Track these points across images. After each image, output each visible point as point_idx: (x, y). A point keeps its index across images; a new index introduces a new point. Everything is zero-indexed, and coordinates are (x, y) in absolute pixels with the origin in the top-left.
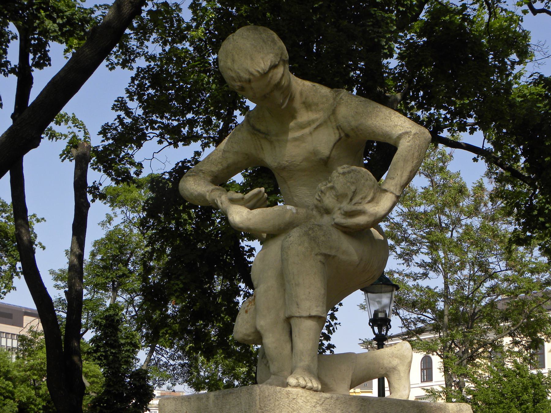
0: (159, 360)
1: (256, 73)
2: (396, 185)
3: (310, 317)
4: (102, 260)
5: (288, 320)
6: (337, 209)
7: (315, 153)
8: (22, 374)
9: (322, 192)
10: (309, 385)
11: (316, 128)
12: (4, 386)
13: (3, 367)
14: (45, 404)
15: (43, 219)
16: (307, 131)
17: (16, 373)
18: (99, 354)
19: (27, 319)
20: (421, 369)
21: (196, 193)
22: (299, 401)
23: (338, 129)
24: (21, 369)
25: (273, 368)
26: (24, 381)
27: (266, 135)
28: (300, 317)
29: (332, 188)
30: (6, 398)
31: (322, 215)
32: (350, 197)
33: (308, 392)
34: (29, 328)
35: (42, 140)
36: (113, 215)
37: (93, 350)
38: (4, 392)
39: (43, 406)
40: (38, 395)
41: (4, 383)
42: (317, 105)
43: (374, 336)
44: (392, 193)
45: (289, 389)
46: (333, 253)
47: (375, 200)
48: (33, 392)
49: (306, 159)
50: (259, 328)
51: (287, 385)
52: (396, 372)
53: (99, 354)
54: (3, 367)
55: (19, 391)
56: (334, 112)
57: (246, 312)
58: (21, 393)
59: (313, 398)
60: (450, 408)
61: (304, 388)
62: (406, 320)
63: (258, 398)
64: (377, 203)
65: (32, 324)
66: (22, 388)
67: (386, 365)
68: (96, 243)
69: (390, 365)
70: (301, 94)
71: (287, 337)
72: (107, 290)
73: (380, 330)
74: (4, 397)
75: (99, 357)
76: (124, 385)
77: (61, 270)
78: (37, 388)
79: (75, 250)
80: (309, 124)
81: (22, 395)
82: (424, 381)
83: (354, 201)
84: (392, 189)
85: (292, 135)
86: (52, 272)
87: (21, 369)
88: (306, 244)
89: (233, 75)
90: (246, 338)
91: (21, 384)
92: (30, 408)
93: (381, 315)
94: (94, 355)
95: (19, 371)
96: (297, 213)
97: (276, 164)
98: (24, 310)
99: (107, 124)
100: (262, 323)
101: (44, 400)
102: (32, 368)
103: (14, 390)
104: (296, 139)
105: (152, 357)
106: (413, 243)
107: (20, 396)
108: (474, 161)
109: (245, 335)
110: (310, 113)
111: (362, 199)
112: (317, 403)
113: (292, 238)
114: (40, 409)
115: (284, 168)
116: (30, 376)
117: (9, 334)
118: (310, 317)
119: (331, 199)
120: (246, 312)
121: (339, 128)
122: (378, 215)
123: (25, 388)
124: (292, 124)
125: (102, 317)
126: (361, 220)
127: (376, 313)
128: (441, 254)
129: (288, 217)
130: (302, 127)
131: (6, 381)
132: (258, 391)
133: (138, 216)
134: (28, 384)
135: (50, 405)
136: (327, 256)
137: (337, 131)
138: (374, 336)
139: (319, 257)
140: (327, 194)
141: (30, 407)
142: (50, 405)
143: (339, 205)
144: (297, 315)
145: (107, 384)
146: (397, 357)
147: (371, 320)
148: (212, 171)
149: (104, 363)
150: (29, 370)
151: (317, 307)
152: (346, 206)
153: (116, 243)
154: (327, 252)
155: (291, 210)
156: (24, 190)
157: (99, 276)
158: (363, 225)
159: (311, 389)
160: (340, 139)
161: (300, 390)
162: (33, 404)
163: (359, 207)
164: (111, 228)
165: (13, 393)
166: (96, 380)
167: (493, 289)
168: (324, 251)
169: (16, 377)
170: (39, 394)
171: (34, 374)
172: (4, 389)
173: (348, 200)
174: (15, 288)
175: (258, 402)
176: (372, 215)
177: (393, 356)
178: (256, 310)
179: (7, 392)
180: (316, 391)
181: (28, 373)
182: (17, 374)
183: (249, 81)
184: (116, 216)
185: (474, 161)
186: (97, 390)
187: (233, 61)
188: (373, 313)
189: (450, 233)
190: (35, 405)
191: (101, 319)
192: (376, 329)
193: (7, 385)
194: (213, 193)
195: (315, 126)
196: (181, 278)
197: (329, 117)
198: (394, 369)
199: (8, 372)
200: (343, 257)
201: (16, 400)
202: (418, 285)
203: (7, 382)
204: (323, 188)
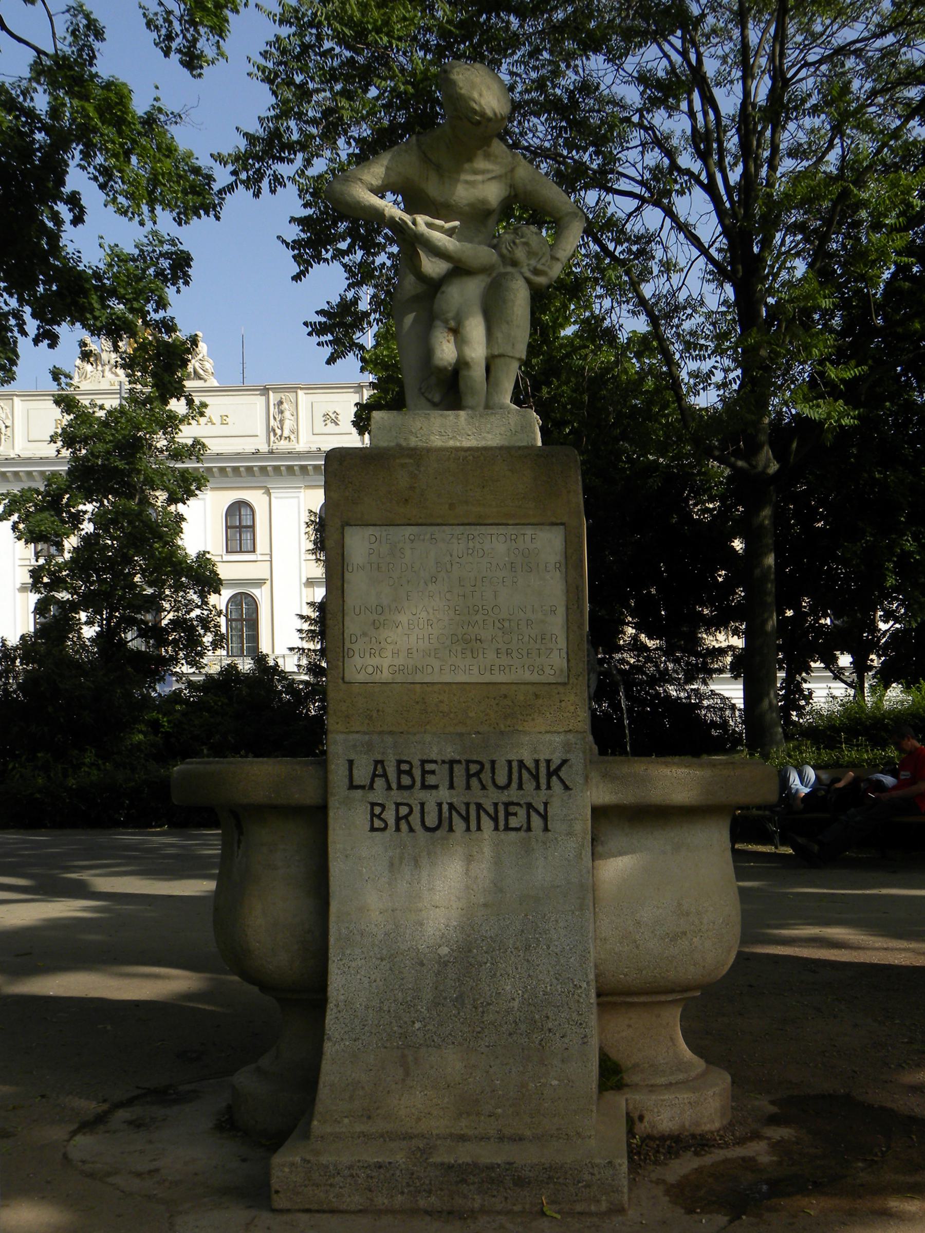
7: (484, 202)
11: (490, 179)
15: (140, 7)
16: (479, 178)
21: (367, 203)
23: (511, 186)
28: (512, 357)
42: (496, 157)
49: (471, 205)
56: (512, 170)
80: (483, 172)
89: (477, 107)
97: (442, 200)
104: (467, 182)
108: (82, 221)
110: (487, 163)
124: (467, 166)
130: (475, 172)
137: (508, 189)
140: (520, 248)
156: (123, 1001)
174: (140, 7)
185: (82, 221)
195: (489, 176)
197: (506, 174)
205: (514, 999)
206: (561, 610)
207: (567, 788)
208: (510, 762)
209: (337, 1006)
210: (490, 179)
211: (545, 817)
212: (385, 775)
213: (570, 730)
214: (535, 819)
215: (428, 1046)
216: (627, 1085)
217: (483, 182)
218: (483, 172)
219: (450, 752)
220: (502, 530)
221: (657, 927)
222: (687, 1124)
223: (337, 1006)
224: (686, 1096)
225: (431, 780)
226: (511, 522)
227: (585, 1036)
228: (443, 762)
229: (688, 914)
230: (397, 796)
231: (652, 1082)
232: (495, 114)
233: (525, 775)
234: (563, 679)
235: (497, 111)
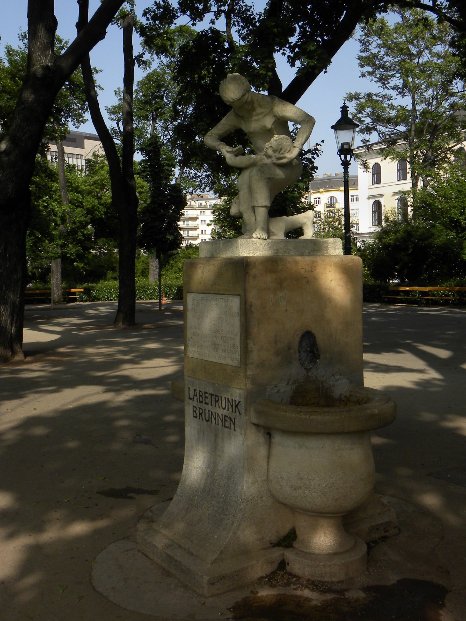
0: (190, 173)
1: (236, 99)
2: (299, 144)
3: (262, 206)
4: (144, 96)
5: (253, 207)
6: (273, 156)
8: (88, 187)
9: (267, 148)
10: (262, 237)
12: (75, 198)
13: (74, 183)
14: (105, 210)
16: (261, 116)
17: (83, 187)
18: (146, 173)
19: (87, 142)
20: (398, 170)
22: (258, 244)
24: (87, 184)
25: (248, 228)
26: (89, 193)
27: (242, 117)
28: (258, 206)
29: (271, 147)
30: (77, 207)
31: (268, 159)
32: (279, 151)
33: (261, 240)
34: (92, 153)
35: (106, 34)
36: (151, 61)
37: (142, 171)
38: (76, 203)
39: (104, 211)
40: (100, 204)
41: (75, 196)
43: (342, 162)
44: (298, 148)
45: (253, 239)
46: (272, 176)
47: (291, 151)
48: (96, 201)
50: (241, 211)
51: (252, 237)
52: (306, 225)
53: (146, 173)
54: (74, 183)
55: (87, 201)
57: (235, 203)
58: (88, 202)
59: (264, 242)
60: (330, 241)
61: (259, 238)
62: (383, 133)
63: (240, 244)
64: (292, 152)
65: (94, 150)
66: (89, 199)
67: (301, 222)
68: (139, 83)
69: (303, 222)
70: (257, 100)
71: (253, 214)
72: (147, 120)
73: (346, 157)
74: (76, 206)
75: (146, 175)
76: (165, 196)
77: (113, 107)
78: (99, 198)
79: (126, 98)
80: (262, 113)
81: (89, 204)
82: (400, 180)
83: (281, 153)
84: (298, 146)
85: (254, 118)
86: (107, 109)
87: (87, 184)
88: (259, 175)
89: (226, 100)
90: (235, 215)
91: (88, 196)
92: (96, 214)
93: (346, 147)
94: (143, 174)
95: (85, 186)
96: (256, 158)
98: (84, 135)
99: (148, 9)
100: (242, 209)
101: (104, 207)
102: (95, 182)
103: (82, 200)
104: (256, 120)
105: (184, 171)
106: (387, 69)
107: (87, 205)
109: (235, 213)
111: (284, 151)
112: (265, 244)
113: (253, 173)
114: (102, 214)
115: (251, 133)
116: (93, 189)
117: (74, 154)
118: (262, 206)
119: (271, 152)
120: (235, 203)
121: (275, 116)
122: (292, 158)
123: (90, 199)
124: (254, 113)
125: (146, 145)
126: (284, 161)
127: (343, 145)
128: (410, 79)
129: (252, 161)
130: (258, 115)
131: (77, 194)
132: (240, 242)
133: (170, 60)
134: (92, 195)
135: (109, 211)
136: (269, 179)
137: (274, 117)
138: (342, 162)
139: (265, 180)
140: (269, 149)
141: (95, 213)
142: (109, 211)
143: (275, 154)
144: (257, 205)
145: (152, 196)
146: (306, 218)
147: (339, 151)
148: (218, 134)
149: (149, 180)
150: (93, 185)
151: (265, 202)
152: (278, 155)
153: (154, 82)
154: (269, 177)
155: (253, 157)
157: (142, 109)
158: (285, 163)
159: (262, 239)
160: (275, 121)
161: (258, 240)
162: (97, 211)
163: (283, 156)
164: (150, 71)
165: (81, 203)
166: (142, 190)
167: (452, 106)
168: (268, 176)
169: (84, 190)
170: (101, 202)
171: (96, 188)
172: (76, 200)
173: (278, 152)
175: (240, 246)
176: (289, 158)
177: (304, 217)
178: (239, 202)
179: (78, 203)
180: (265, 239)
181: (92, 187)
182: (85, 188)
183: (233, 102)
184: (153, 61)
186: (144, 198)
187: (226, 94)
188: (340, 145)
189: (417, 59)
190: (99, 212)
191: (146, 146)
192: (343, 157)
193: (78, 197)
194: (219, 146)
195: (263, 115)
196: (204, 120)
198: (305, 223)
199: (78, 187)
200: (278, 177)
201: (85, 208)
202: (392, 104)
203: (77, 195)
204: (267, 147)
205: (221, 498)
206: (239, 334)
207: (240, 414)
208: (225, 398)
209: (182, 482)
210: (265, 115)
211: (234, 424)
212: (196, 396)
213: (241, 389)
214: (232, 424)
215: (195, 507)
216: (293, 547)
217: (262, 118)
218: (262, 113)
219: (211, 392)
220: (223, 297)
221: (288, 482)
222: (306, 574)
223: (182, 482)
224: (306, 561)
225: (207, 402)
226: (226, 293)
227: (234, 522)
228: (210, 394)
229: (302, 479)
230: (200, 405)
231: (302, 550)
232: (233, 100)
233: (229, 405)
234: (239, 366)
235: (234, 98)
